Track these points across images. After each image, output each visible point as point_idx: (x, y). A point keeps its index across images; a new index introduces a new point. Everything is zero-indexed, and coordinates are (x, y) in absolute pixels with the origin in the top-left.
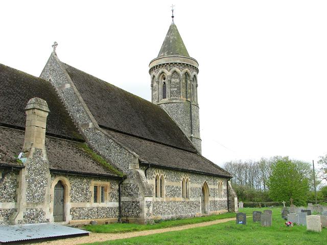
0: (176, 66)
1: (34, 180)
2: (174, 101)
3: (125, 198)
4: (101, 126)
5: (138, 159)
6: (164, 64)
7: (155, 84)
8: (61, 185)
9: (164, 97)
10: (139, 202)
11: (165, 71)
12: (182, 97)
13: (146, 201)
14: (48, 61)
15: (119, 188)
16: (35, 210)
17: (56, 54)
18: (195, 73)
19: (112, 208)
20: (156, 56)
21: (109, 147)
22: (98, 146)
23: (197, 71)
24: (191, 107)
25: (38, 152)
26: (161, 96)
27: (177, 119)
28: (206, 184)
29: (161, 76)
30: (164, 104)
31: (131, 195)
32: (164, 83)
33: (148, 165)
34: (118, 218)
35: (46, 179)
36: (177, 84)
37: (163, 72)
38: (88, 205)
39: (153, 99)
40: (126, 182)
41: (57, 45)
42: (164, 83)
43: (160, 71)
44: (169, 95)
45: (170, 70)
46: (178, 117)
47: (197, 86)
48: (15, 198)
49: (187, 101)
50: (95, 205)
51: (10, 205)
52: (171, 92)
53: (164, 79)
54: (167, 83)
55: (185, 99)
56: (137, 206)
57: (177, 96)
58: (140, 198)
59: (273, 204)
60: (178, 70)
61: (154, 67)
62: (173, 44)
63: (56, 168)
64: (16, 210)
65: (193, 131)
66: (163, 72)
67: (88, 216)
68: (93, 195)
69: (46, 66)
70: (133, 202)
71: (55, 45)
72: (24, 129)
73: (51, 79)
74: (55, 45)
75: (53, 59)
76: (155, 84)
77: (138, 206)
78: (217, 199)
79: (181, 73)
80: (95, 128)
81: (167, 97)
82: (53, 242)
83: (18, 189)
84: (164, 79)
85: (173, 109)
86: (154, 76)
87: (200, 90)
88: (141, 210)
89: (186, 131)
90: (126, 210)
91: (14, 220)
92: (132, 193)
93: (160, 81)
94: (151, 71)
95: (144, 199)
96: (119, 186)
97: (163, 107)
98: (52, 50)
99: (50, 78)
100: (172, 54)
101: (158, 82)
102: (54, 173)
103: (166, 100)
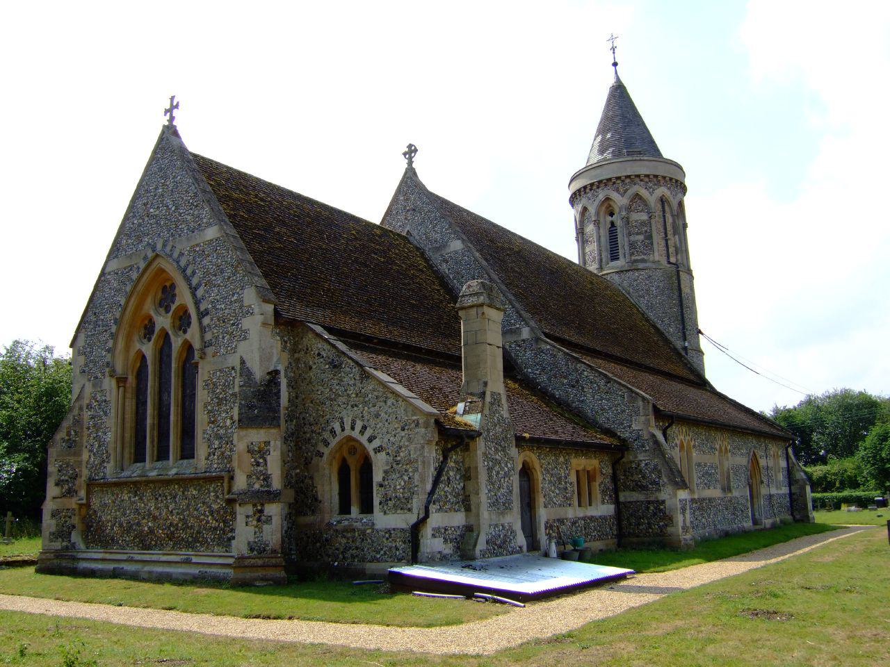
0: (634, 181)
3: (627, 493)
4: (547, 335)
5: (651, 405)
6: (609, 180)
7: (590, 228)
8: (526, 472)
9: (614, 257)
10: (663, 502)
11: (615, 196)
12: (656, 254)
16: (501, 527)
21: (577, 382)
22: (549, 379)
23: (683, 189)
25: (496, 400)
26: (606, 255)
27: (651, 307)
28: (754, 461)
32: (612, 224)
36: (643, 224)
37: (608, 199)
40: (629, 457)
41: (405, 154)
42: (612, 224)
43: (601, 197)
44: (627, 252)
45: (626, 191)
53: (612, 214)
54: (619, 223)
56: (661, 514)
58: (664, 495)
59: (849, 501)
60: (644, 192)
62: (623, 122)
64: (469, 529)
65: (687, 333)
66: (608, 199)
68: (576, 493)
70: (649, 502)
71: (411, 152)
74: (411, 152)
75: (410, 182)
76: (590, 228)
77: (661, 510)
78: (773, 491)
82: (554, 603)
84: (612, 214)
86: (585, 209)
88: (669, 520)
89: (671, 331)
92: (644, 482)
93: (602, 219)
94: (574, 199)
95: (675, 495)
98: (403, 164)
101: (597, 223)
103: (621, 263)
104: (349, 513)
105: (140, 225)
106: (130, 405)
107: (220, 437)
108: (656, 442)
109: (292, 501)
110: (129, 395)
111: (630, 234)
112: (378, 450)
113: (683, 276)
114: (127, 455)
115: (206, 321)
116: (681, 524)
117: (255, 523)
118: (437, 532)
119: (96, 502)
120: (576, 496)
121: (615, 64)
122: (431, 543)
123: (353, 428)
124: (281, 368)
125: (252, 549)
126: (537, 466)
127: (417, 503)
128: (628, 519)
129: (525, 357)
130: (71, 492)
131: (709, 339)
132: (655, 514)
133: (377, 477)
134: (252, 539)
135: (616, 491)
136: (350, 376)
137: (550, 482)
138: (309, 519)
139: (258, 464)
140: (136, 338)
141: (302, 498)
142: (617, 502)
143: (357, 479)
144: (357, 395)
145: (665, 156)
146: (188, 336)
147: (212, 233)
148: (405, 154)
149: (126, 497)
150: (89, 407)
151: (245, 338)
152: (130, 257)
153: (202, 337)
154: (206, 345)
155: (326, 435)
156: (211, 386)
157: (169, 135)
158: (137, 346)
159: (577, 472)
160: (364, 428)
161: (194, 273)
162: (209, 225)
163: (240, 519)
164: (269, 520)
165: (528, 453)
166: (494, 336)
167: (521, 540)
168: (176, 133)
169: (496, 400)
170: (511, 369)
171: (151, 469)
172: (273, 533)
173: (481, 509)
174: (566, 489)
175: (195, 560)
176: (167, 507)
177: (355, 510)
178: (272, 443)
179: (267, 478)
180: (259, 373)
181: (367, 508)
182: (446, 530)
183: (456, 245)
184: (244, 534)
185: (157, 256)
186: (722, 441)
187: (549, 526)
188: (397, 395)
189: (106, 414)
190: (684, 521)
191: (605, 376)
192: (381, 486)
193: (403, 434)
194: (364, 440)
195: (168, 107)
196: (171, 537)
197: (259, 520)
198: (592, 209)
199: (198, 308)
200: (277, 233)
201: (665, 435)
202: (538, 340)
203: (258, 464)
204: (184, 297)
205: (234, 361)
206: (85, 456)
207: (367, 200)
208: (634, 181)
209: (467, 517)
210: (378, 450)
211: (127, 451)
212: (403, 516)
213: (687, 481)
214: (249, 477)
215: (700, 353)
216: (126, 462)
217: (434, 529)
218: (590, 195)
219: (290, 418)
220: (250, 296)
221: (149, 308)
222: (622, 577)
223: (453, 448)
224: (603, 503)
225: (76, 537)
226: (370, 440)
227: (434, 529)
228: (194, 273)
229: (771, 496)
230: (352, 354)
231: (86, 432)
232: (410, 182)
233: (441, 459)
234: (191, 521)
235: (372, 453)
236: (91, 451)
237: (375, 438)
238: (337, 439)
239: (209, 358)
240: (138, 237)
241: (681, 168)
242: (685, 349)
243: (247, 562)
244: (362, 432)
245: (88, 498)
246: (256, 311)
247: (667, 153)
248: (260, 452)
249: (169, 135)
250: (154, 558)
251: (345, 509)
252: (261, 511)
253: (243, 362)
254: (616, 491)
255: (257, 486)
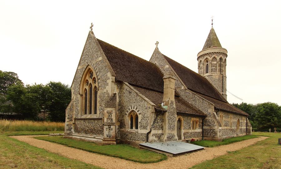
0: (214, 52)
1: (171, 118)
2: (213, 74)
3: (205, 127)
4: (188, 89)
6: (207, 54)
7: (201, 65)
8: (179, 121)
9: (207, 72)
10: (215, 130)
11: (209, 57)
13: (217, 128)
14: (154, 53)
15: (202, 122)
17: (158, 49)
18: (225, 57)
19: (199, 132)
20: (201, 50)
21: (195, 100)
22: (188, 99)
23: (227, 56)
24: (223, 79)
26: (205, 72)
29: (205, 61)
30: (206, 75)
31: (209, 126)
32: (207, 64)
33: (219, 109)
34: (202, 138)
35: (175, 118)
36: (215, 64)
38: (190, 131)
39: (199, 71)
40: (207, 118)
42: (207, 64)
43: (205, 58)
45: (211, 56)
46: (216, 86)
47: (226, 66)
48: (162, 128)
49: (221, 74)
50: (193, 131)
51: (160, 132)
52: (211, 69)
53: (207, 62)
54: (209, 64)
55: (220, 73)
57: (215, 72)
58: (216, 128)
60: (216, 57)
61: (201, 56)
62: (212, 41)
63: (179, 112)
64: (163, 134)
66: (207, 58)
67: (190, 137)
69: (153, 55)
70: (211, 129)
72: (163, 93)
73: (157, 63)
76: (201, 65)
78: (242, 128)
79: (218, 58)
80: (186, 89)
81: (209, 72)
83: (163, 123)
84: (207, 62)
85: (212, 77)
86: (201, 61)
87: (227, 67)
88: (216, 133)
90: (206, 133)
91: (163, 139)
92: (210, 125)
94: (198, 59)
96: (202, 120)
97: (207, 78)
98: (155, 46)
99: (156, 62)
100: (212, 47)
101: (203, 64)
102: (178, 114)
104: (133, 129)
105: (85, 57)
106: (84, 101)
107: (102, 109)
108: (214, 115)
109: (119, 125)
110: (83, 99)
111: (211, 67)
112: (140, 114)
113: (224, 78)
114: (83, 113)
115: (99, 81)
116: (219, 135)
117: (108, 130)
118: (153, 135)
119: (76, 123)
120: (192, 127)
121: (212, 24)
122: (151, 138)
123: (134, 108)
124: (117, 93)
125: (108, 136)
126: (182, 120)
127: (149, 128)
128: (205, 133)
129: (182, 94)
130: (71, 120)
131: (230, 93)
132: (212, 132)
133: (139, 121)
134: (108, 134)
135: (203, 126)
136: (134, 94)
137: (185, 123)
138: (123, 129)
139: (110, 116)
140: (85, 85)
141: (122, 124)
142: (203, 129)
143: (134, 119)
144: (135, 100)
145: (222, 47)
146: (96, 85)
147: (100, 59)
148: (156, 44)
149: (82, 122)
150: (75, 101)
151: (108, 85)
152: (83, 66)
153: (98, 85)
154: (99, 87)
155: (128, 110)
156: (100, 97)
157: (91, 33)
158: (85, 87)
159: (193, 121)
160: (137, 108)
161: (97, 69)
162: (100, 57)
163: (105, 129)
164: (112, 129)
165: (180, 116)
166: (173, 86)
167: (176, 137)
168: (93, 33)
169: (172, 103)
170: (177, 96)
171: (89, 116)
172: (113, 133)
173: (166, 130)
174: (190, 125)
175: (96, 137)
176: (91, 125)
177: (134, 128)
178: (113, 111)
179: (112, 119)
180: (111, 94)
181: (137, 128)
182: (156, 134)
183: (167, 66)
184: (106, 132)
185: (88, 65)
186: (231, 116)
187: (184, 134)
188: (145, 100)
189: (78, 103)
190: (220, 135)
191: (202, 99)
192: (140, 123)
193: (146, 110)
194: (136, 111)
195: (91, 26)
196: (91, 132)
197: (109, 129)
198: (203, 60)
199: (97, 78)
200: (116, 57)
201: (216, 113)
202: (186, 89)
203: (110, 116)
204: (95, 75)
205: (105, 91)
206: (74, 112)
207: (146, 56)
208: (214, 52)
209: (162, 131)
210: (140, 114)
211: (83, 112)
212: (145, 130)
213: (221, 124)
214: (107, 119)
215: (226, 95)
216: (83, 114)
217: (152, 134)
218: (202, 57)
219: (119, 105)
220: (109, 74)
221: (87, 78)
222: (202, 149)
223: (159, 114)
224: (199, 129)
225: (73, 130)
226: (138, 111)
227: (152, 134)
228: (97, 69)
229: (241, 129)
230: (135, 90)
231: (74, 107)
232: (157, 52)
233: (156, 117)
234: (96, 128)
235: (138, 115)
236: (75, 111)
237: (139, 111)
238: (130, 111)
239: (100, 90)
240: (85, 60)
241: (227, 50)
242: (223, 94)
243: (106, 139)
244: (136, 109)
245: (75, 122)
246: (111, 78)
247: (223, 46)
248: (110, 113)
249: (91, 33)
250: (88, 136)
251: (132, 128)
252: (110, 127)
253: (107, 91)
254: (203, 126)
255: (109, 121)
